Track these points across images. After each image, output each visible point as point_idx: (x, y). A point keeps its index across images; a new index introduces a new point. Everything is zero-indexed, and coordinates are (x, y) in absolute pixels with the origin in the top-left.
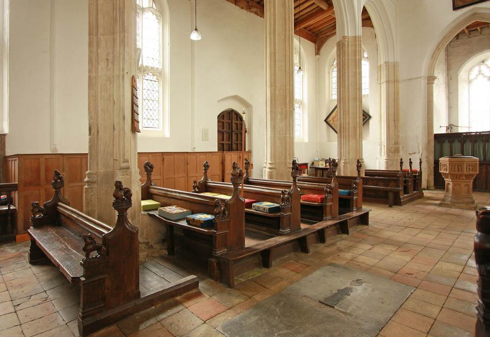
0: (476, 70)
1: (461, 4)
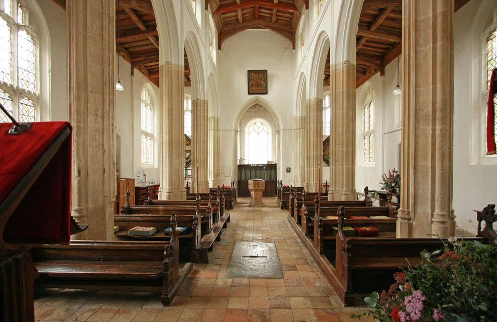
0: (251, 128)
1: (252, 92)
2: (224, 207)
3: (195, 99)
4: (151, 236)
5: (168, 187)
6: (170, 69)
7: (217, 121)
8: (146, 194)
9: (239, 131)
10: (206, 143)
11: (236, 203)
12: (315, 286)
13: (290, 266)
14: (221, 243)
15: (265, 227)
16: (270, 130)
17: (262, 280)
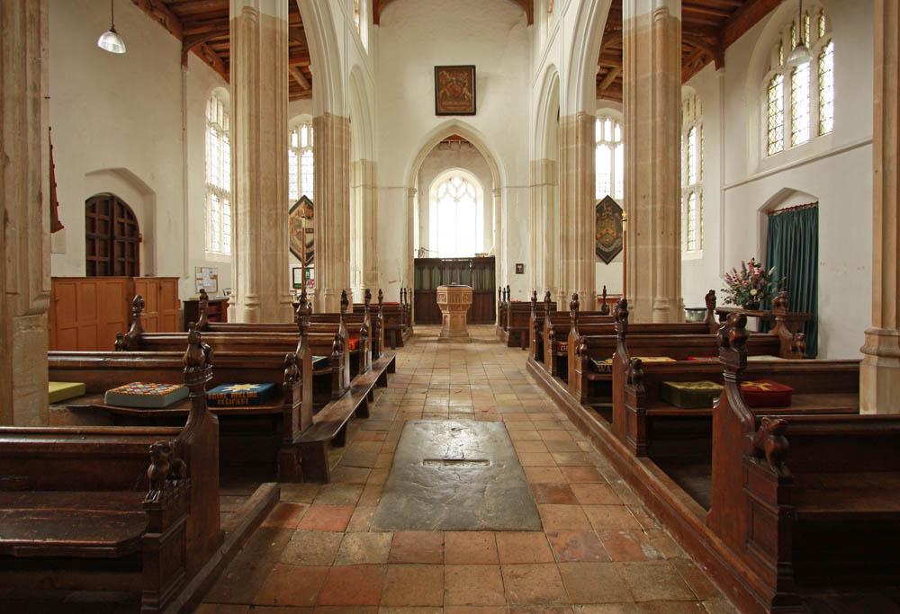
1: (443, 110)
2: (381, 339)
3: (322, 114)
4: (167, 407)
5: (248, 294)
6: (253, 26)
7: (370, 169)
8: (209, 310)
9: (418, 188)
10: (345, 206)
11: (412, 335)
12: (645, 559)
13: (555, 490)
14: (371, 422)
15: (476, 384)
16: (480, 191)
17: (481, 538)
